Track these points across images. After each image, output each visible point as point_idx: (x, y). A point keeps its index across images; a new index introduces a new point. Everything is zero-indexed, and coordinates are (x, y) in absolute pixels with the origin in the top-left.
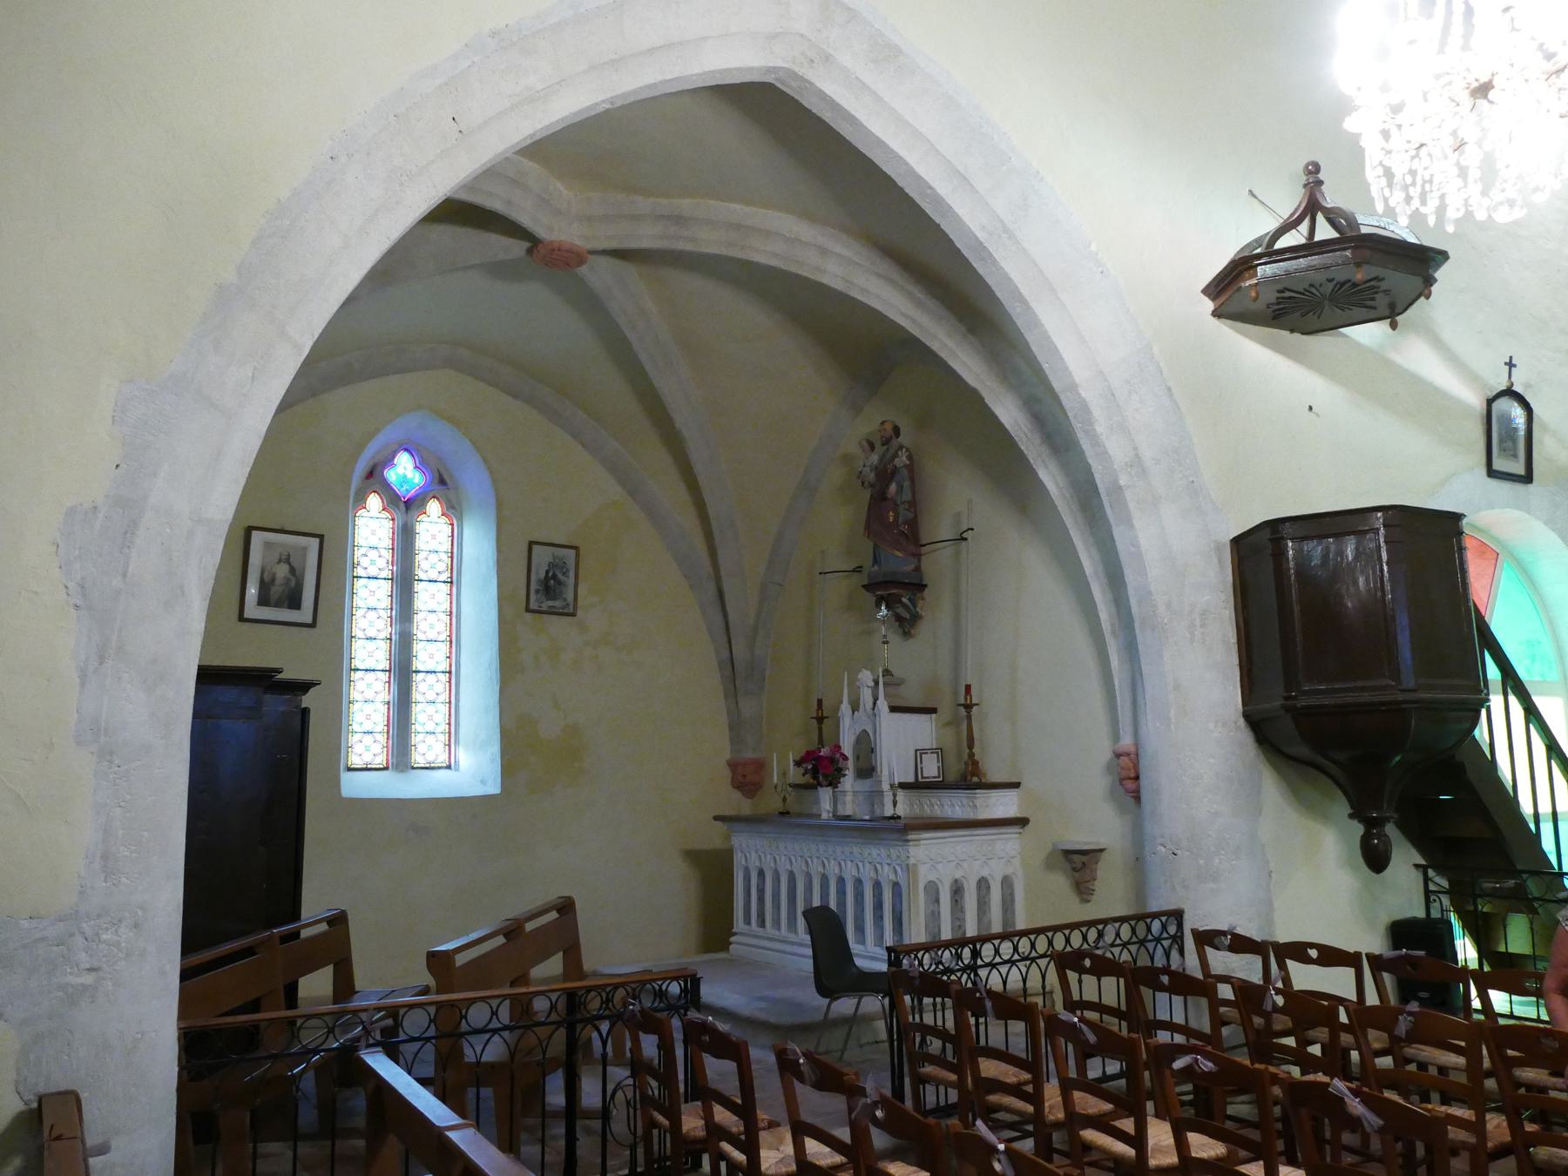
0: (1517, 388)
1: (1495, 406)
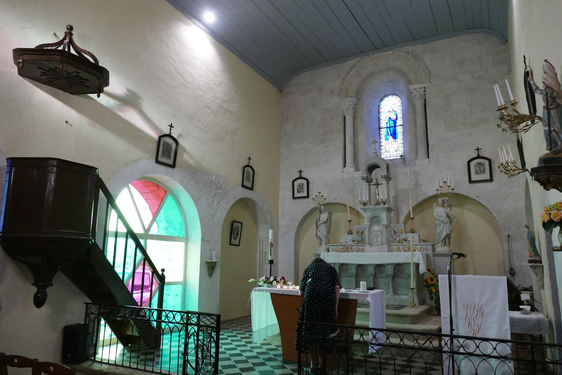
0: (483, 154)
1: (295, 182)
